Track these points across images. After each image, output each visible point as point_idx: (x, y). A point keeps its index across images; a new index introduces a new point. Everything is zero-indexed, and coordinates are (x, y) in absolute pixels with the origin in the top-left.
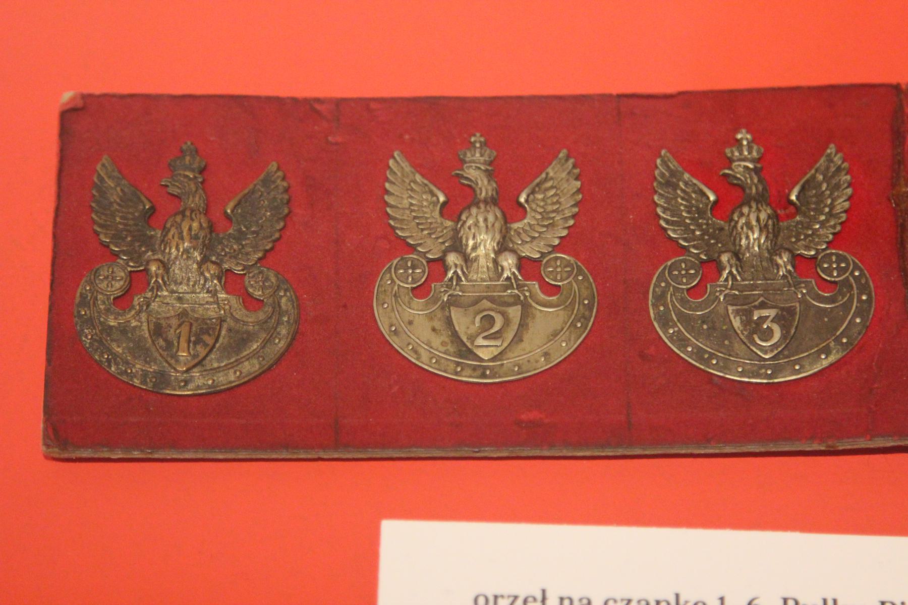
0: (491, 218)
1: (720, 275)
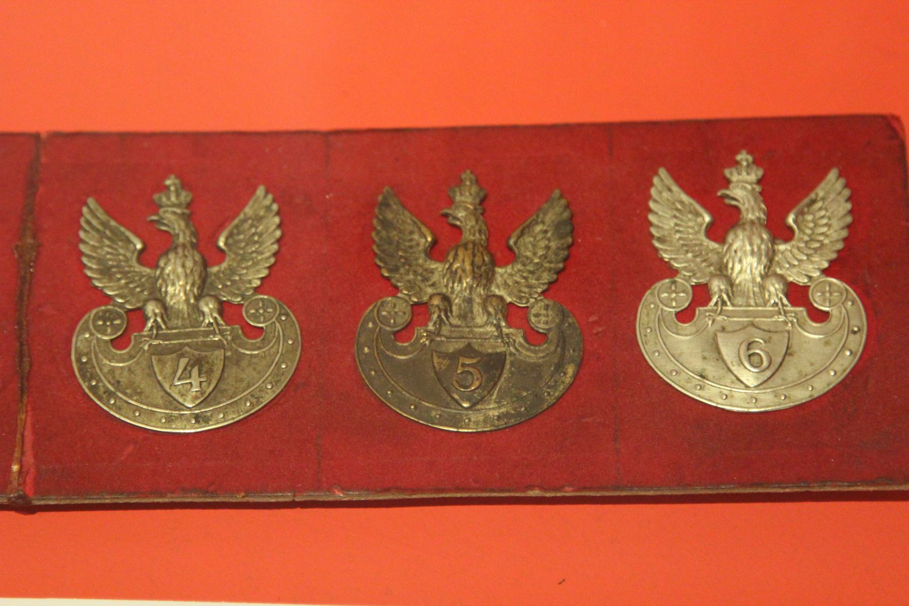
0: (189, 264)
1: (144, 325)
